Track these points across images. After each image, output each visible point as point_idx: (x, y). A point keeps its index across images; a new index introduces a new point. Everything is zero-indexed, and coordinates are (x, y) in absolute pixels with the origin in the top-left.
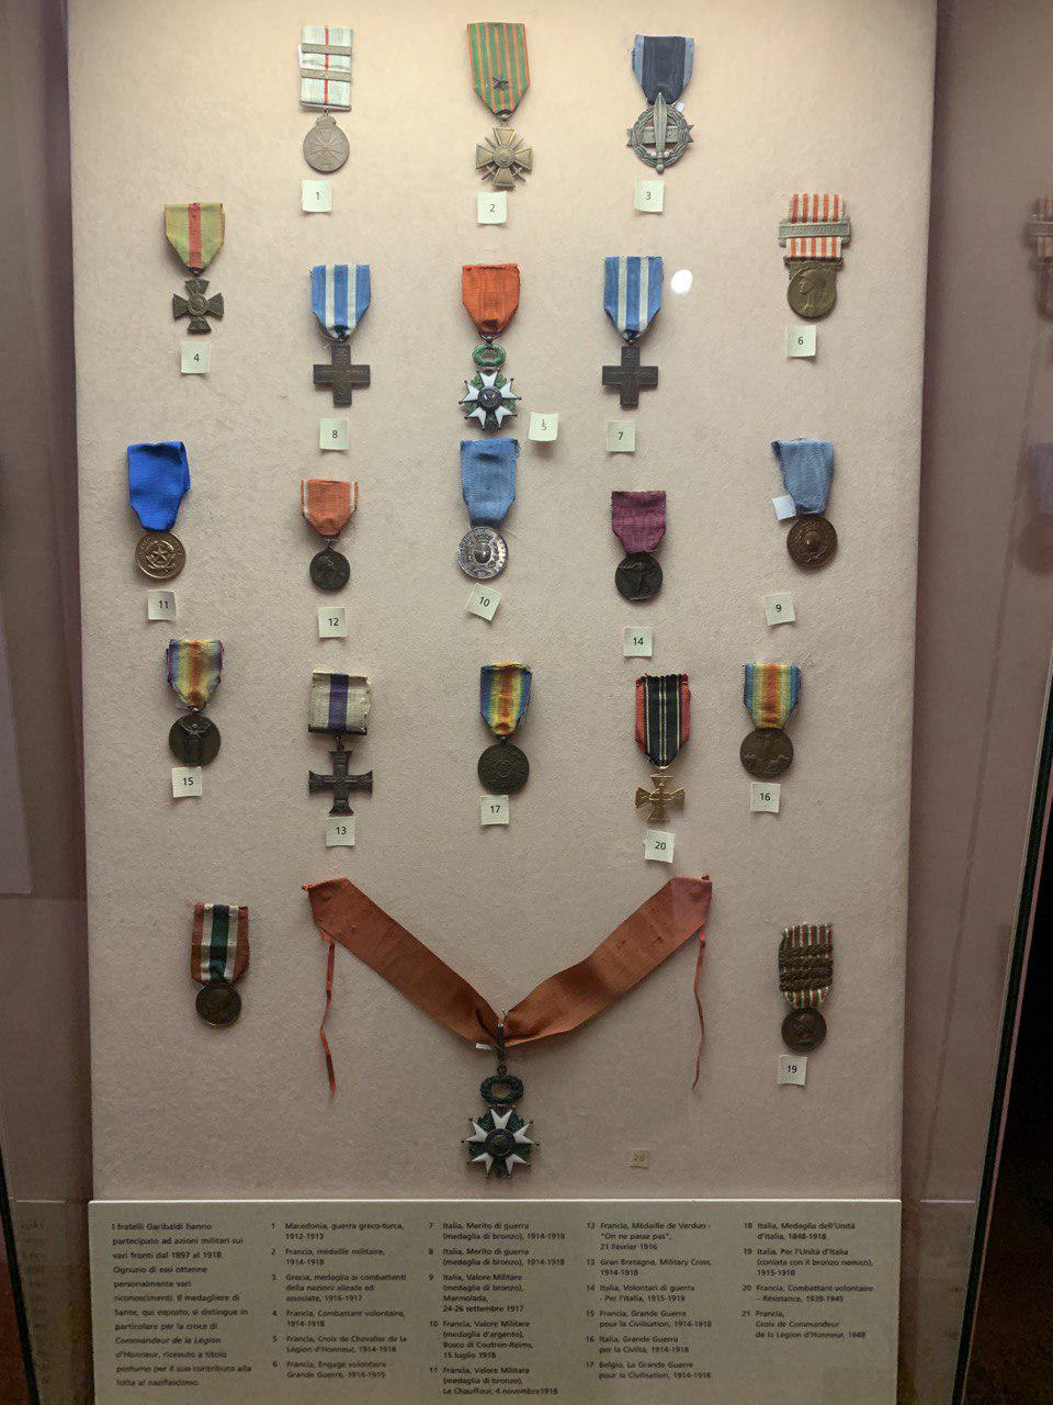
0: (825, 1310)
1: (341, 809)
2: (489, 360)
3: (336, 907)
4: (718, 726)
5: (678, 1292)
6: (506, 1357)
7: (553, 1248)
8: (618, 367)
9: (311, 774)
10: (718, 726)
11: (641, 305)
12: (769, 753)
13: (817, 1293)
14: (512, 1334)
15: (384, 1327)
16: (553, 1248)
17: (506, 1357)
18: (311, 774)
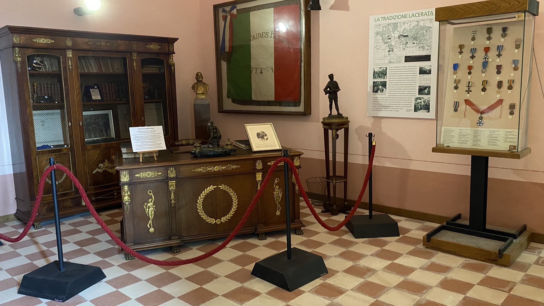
0: (511, 140)
1: (468, 93)
2: (486, 55)
3: (467, 102)
4: (505, 85)
5: (496, 137)
6: (479, 143)
7: (484, 133)
8: (273, 101)
9: (176, 39)
10: (505, 85)
11: (262, 110)
12: (510, 88)
13: (511, 138)
14: (480, 141)
15: (467, 139)
16: (484, 133)
17: (479, 143)
18: (176, 39)
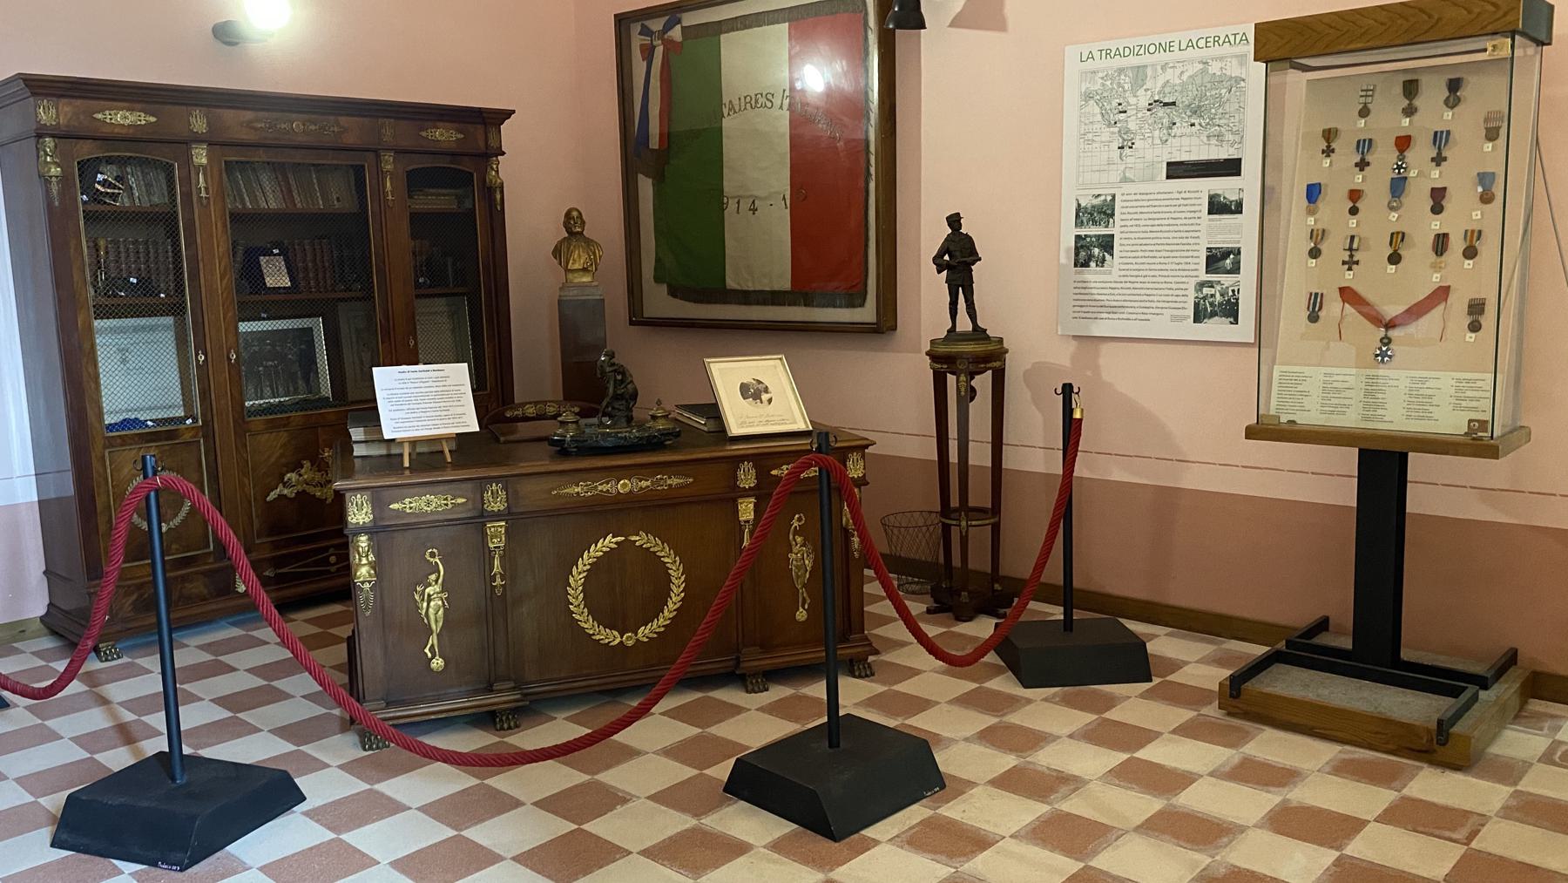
0: (1474, 404)
1: (1350, 269)
2: (1402, 157)
3: (1347, 294)
4: (1457, 245)
5: (1430, 397)
6: (1380, 412)
7: (1395, 383)
8: (786, 292)
9: (508, 114)
10: (1457, 245)
11: (754, 318)
12: (1470, 253)
13: (1472, 399)
14: (1382, 406)
15: (1346, 402)
16: (1395, 383)
17: (1380, 412)
18: (508, 114)
